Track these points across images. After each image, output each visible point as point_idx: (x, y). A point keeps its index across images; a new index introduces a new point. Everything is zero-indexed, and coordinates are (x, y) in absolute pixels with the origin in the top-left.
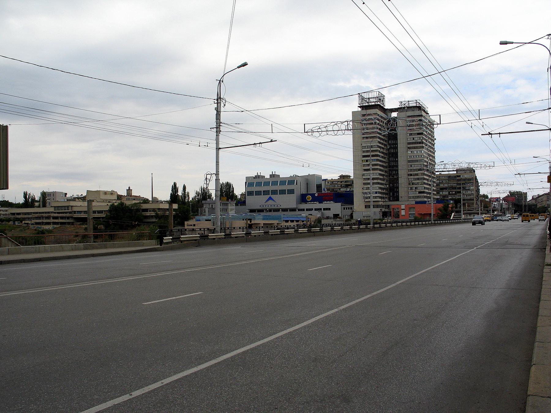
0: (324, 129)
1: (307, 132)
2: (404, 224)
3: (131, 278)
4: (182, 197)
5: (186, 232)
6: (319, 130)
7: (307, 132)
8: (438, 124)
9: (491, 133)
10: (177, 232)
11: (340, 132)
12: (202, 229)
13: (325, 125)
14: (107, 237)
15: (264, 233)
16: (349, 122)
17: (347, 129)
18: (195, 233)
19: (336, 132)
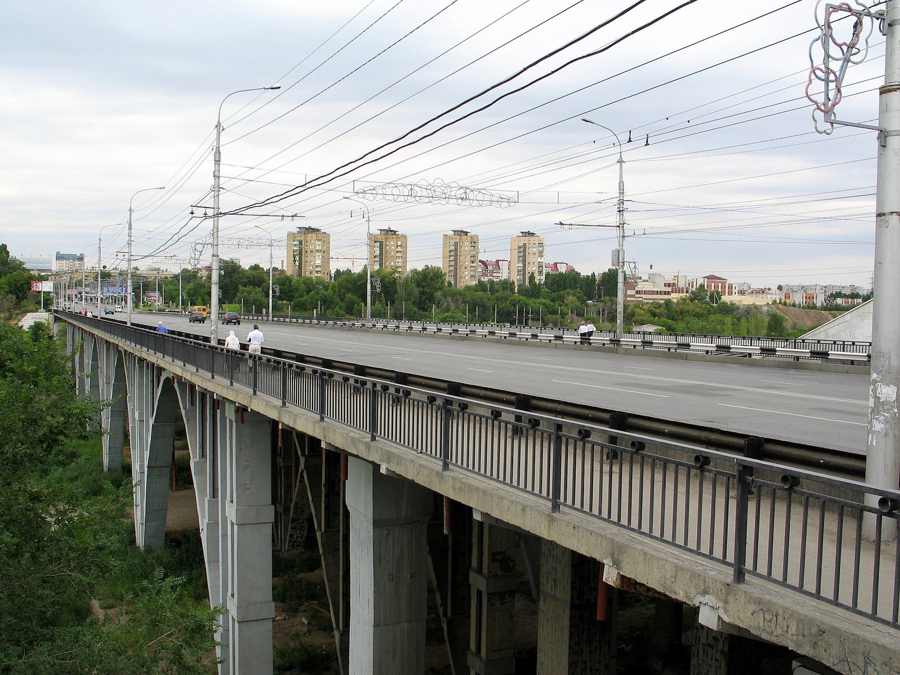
0: (380, 191)
6: (374, 192)
8: (516, 202)
16: (412, 186)
17: (410, 195)
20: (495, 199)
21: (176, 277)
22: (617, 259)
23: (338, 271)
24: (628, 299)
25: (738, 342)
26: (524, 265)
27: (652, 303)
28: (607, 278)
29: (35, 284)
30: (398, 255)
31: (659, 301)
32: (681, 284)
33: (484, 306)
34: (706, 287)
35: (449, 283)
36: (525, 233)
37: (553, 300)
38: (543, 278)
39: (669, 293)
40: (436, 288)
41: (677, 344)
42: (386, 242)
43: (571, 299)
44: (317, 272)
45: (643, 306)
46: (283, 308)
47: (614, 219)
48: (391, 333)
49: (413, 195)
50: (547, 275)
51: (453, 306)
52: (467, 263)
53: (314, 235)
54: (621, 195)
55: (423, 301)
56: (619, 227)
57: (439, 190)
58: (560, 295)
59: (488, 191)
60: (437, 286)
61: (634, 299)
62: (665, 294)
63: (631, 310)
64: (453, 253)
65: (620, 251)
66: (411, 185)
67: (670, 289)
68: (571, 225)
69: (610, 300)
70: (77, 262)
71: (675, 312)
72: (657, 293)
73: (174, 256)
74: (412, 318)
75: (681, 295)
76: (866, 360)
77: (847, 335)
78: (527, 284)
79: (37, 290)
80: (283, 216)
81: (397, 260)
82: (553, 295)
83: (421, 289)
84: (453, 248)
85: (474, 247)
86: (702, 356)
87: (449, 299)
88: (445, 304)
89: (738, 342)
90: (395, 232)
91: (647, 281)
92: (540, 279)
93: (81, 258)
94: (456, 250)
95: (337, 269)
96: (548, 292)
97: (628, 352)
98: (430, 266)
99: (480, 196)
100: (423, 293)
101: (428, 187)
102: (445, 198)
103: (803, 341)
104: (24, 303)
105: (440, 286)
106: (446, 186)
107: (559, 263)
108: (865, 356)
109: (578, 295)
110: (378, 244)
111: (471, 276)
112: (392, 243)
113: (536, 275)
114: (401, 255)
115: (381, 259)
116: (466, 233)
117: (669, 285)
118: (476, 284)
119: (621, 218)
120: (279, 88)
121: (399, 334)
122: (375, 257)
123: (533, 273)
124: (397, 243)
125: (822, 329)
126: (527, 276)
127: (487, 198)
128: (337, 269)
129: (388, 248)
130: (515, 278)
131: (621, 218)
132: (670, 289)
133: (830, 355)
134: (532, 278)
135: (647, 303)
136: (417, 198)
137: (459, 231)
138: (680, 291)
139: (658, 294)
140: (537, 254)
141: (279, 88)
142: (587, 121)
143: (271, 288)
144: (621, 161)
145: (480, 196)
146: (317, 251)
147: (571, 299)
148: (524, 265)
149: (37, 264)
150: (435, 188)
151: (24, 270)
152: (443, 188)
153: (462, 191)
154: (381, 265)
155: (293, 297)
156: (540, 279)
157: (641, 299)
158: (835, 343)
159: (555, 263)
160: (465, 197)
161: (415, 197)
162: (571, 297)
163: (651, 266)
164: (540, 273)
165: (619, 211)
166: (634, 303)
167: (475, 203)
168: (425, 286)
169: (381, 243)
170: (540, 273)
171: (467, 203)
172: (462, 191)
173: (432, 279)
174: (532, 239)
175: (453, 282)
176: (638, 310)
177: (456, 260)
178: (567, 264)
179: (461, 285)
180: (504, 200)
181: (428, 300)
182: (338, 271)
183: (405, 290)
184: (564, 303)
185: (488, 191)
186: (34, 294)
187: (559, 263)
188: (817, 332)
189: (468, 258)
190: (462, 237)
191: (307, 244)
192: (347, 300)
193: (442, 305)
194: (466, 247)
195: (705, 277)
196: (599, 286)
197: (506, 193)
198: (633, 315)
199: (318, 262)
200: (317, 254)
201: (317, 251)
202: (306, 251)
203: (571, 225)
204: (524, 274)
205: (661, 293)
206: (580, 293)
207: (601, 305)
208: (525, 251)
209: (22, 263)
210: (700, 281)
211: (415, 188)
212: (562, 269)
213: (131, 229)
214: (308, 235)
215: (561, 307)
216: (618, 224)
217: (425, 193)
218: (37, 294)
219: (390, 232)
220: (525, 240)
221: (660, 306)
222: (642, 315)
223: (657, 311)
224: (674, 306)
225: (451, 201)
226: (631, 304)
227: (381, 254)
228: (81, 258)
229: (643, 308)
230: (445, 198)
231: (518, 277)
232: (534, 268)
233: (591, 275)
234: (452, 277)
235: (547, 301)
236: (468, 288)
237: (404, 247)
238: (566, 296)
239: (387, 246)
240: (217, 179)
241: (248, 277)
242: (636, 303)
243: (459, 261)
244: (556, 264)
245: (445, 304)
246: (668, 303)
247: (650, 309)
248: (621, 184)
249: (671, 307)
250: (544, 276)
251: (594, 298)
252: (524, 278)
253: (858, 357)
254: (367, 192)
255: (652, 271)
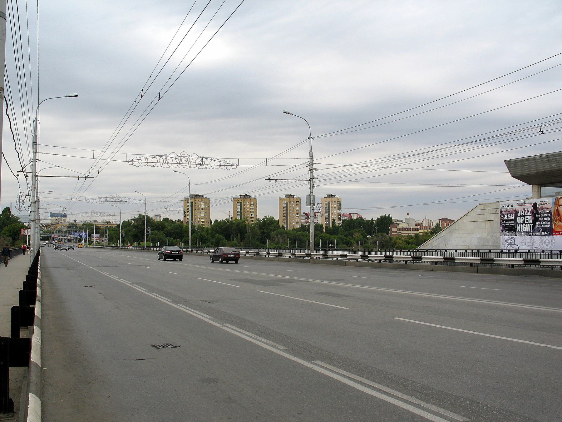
0: (144, 161)
1: (128, 161)
2: (425, 262)
3: (317, 281)
4: (370, 223)
5: (467, 253)
6: (140, 161)
7: (128, 161)
8: (237, 166)
9: (270, 178)
10: (424, 252)
11: (158, 165)
12: (437, 251)
13: (146, 157)
14: (309, 246)
15: (481, 260)
16: (166, 157)
17: (164, 162)
18: (407, 254)
19: (154, 164)
20: (222, 164)
21: (118, 226)
22: (309, 201)
23: (216, 221)
24: (392, 234)
25: (400, 253)
26: (329, 215)
27: (407, 236)
28: (380, 221)
29: (23, 231)
30: (251, 210)
31: (412, 235)
32: (426, 224)
33: (300, 240)
34: (441, 226)
35: (283, 227)
36: (329, 195)
37: (346, 236)
38: (341, 222)
39: (417, 230)
40: (271, 230)
41: (340, 255)
42: (244, 203)
43: (357, 235)
44: (202, 222)
45: (401, 238)
46: (177, 244)
47: (307, 176)
48: (200, 255)
49: (166, 162)
50: (344, 221)
51: (281, 241)
52: (294, 214)
53: (200, 199)
54: (311, 160)
55: (264, 238)
56: (310, 180)
57: (184, 159)
58: (351, 232)
59: (218, 159)
60: (272, 229)
61: (396, 234)
62: (415, 230)
63: (394, 241)
64: (285, 209)
65: (311, 196)
66: (165, 156)
67: (418, 227)
68: (276, 180)
69: (381, 235)
70: (63, 218)
71: (421, 241)
72: (410, 230)
73: (65, 209)
74: (254, 247)
75: (426, 230)
76: (443, 261)
77: (444, 246)
78: (331, 226)
79: (25, 234)
80: (79, 177)
81: (251, 213)
82: (346, 233)
83: (262, 231)
84: (285, 205)
85: (298, 204)
86: (354, 262)
87: (279, 236)
88: (276, 240)
89: (400, 253)
90: (250, 196)
91: (405, 223)
92: (338, 223)
93: (65, 216)
94: (287, 207)
95: (216, 220)
96: (343, 231)
97: (315, 262)
98: (267, 217)
99: (213, 163)
100: (263, 233)
101: (177, 157)
102: (189, 164)
103: (418, 251)
104: (17, 242)
105: (273, 229)
106: (189, 156)
107: (352, 213)
108: (441, 258)
109: (362, 232)
110: (239, 204)
111: (297, 222)
112: (248, 203)
113: (337, 221)
114: (253, 210)
115: (241, 213)
116: (293, 196)
117: (419, 225)
118: (299, 227)
119: (311, 175)
120: (77, 96)
121: (203, 255)
122: (237, 212)
123: (334, 220)
124: (251, 203)
125: (429, 242)
126: (331, 221)
127: (217, 163)
128: (216, 220)
129: (245, 206)
130: (324, 224)
131: (311, 175)
132: (418, 227)
133: (423, 259)
134: (334, 223)
135: (404, 236)
136: (170, 165)
137: (289, 195)
138: (425, 228)
139: (411, 230)
140: (337, 208)
141: (77, 96)
142: (287, 113)
143: (145, 229)
144: (310, 138)
145: (213, 163)
146: (202, 209)
147: (357, 235)
148: (329, 215)
149: (25, 219)
150: (181, 158)
151: (20, 222)
152: (187, 158)
153: (200, 159)
154: (241, 217)
155: (183, 237)
156: (338, 223)
157: (400, 234)
158: (436, 251)
159: (350, 213)
160: (202, 163)
161: (168, 163)
162: (357, 234)
163: (408, 213)
164: (339, 219)
165: (310, 170)
166: (396, 236)
167: (209, 167)
168: (264, 229)
169: (241, 203)
170: (339, 219)
171: (204, 167)
172: (200, 159)
173: (268, 224)
174: (333, 199)
175: (285, 226)
176: (398, 241)
177: (287, 213)
178: (357, 214)
179: (291, 228)
180: (229, 165)
181: (266, 237)
182: (216, 221)
183: (252, 231)
184: (353, 237)
185: (218, 159)
186: (23, 237)
187: (352, 213)
188: (426, 244)
189: (295, 212)
190: (291, 199)
191: (196, 205)
192: (216, 238)
193: (274, 240)
194: (293, 204)
195: (441, 219)
196: (375, 226)
197: (230, 160)
198: (395, 243)
199: (203, 215)
200: (202, 211)
201: (202, 209)
202: (195, 209)
203: (276, 180)
204: (329, 220)
205: (413, 230)
206: (362, 231)
207: (375, 238)
208: (329, 206)
209: (18, 218)
210: (437, 222)
211: (168, 158)
212: (354, 217)
213: (38, 192)
214: (196, 199)
215: (350, 239)
216: (309, 178)
217: (174, 161)
218: (25, 237)
219: (246, 197)
220: (330, 199)
221: (412, 237)
222: (401, 244)
223: (410, 240)
224: (420, 238)
225: (192, 166)
226: (395, 237)
227: (241, 210)
228: (65, 216)
229: (401, 239)
230: (189, 164)
231: (326, 223)
232: (335, 217)
233: (370, 220)
234: (285, 223)
235: (343, 237)
236: (294, 229)
237: (255, 205)
238: (354, 233)
239: (245, 205)
240: (34, 154)
241: (156, 225)
242: (397, 236)
243: (289, 213)
244: (350, 214)
245: (276, 240)
246: (417, 235)
247: (406, 239)
248: (311, 153)
249: (419, 238)
250: (342, 221)
251: (373, 234)
252: (329, 223)
253: (438, 259)
254: (135, 161)
255: (408, 217)
